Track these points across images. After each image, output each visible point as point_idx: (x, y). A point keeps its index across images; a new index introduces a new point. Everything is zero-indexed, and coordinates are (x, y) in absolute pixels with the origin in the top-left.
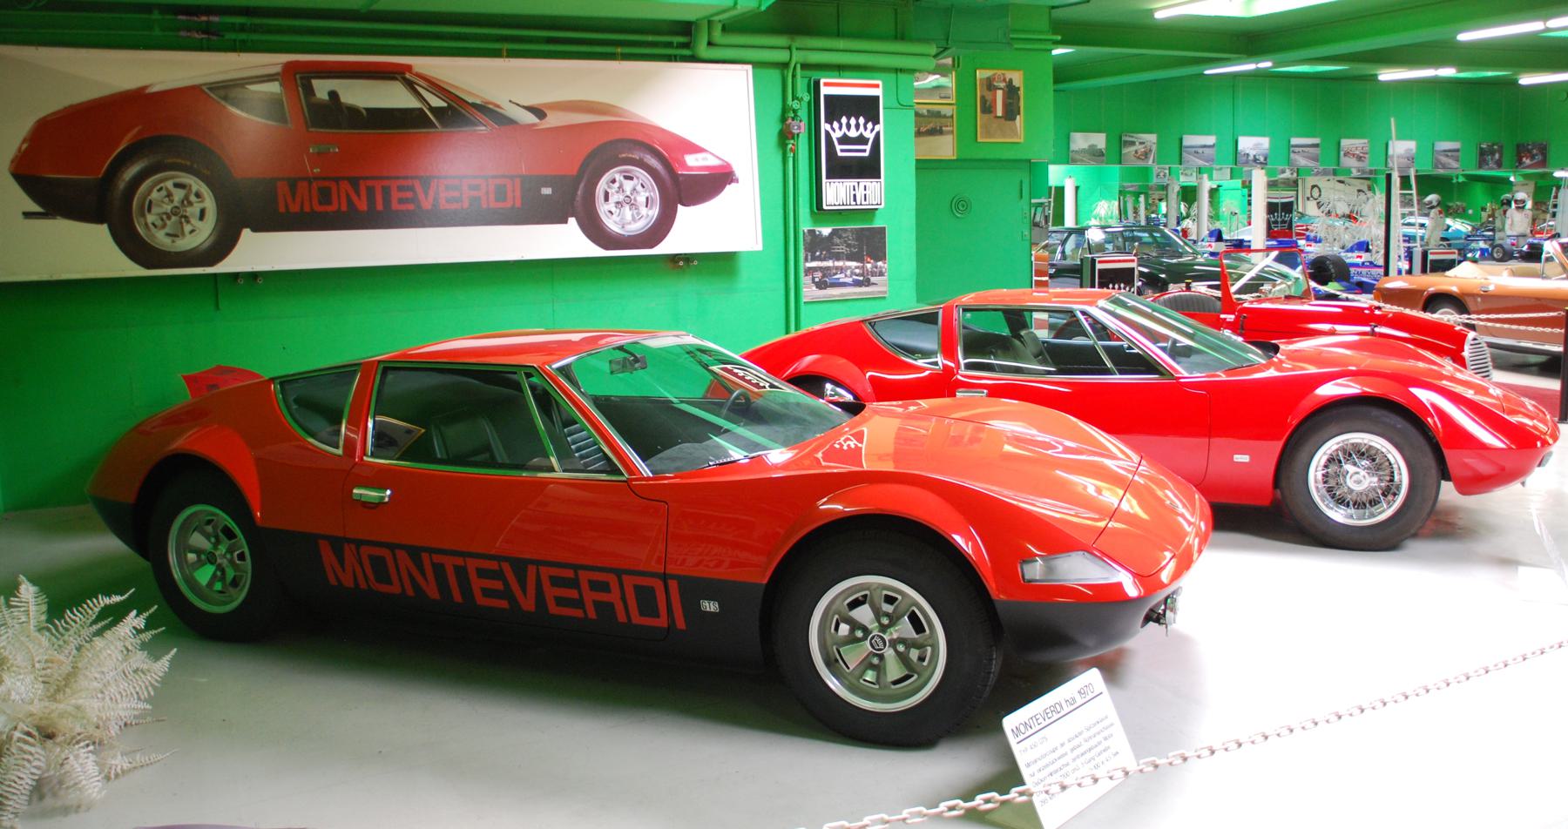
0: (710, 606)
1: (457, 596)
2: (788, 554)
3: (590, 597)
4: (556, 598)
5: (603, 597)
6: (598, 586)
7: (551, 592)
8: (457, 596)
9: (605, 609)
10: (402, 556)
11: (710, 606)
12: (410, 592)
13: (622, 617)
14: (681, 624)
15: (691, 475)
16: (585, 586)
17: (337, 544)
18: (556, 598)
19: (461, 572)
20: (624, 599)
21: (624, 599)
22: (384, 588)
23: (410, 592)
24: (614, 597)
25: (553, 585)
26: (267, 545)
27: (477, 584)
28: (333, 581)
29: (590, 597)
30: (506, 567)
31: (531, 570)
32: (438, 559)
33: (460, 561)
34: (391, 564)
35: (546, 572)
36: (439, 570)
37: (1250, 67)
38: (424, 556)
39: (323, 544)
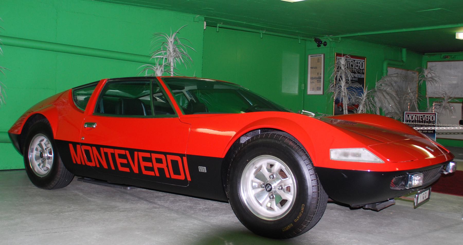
0: (203, 169)
1: (113, 168)
2: (432, 52)
3: (157, 166)
4: (145, 167)
5: (160, 165)
6: (159, 161)
7: (143, 164)
8: (113, 168)
9: (161, 171)
10: (94, 148)
11: (203, 169)
12: (98, 166)
13: (168, 176)
14: (189, 179)
15: (434, 55)
16: (154, 160)
17: (75, 144)
18: (145, 167)
19: (113, 155)
20: (167, 166)
21: (167, 166)
22: (89, 164)
23: (98, 166)
24: (163, 166)
25: (122, 166)
26: (60, 147)
27: (119, 161)
28: (75, 162)
29: (157, 166)
30: (127, 152)
31: (136, 153)
32: (106, 150)
33: (112, 151)
34: (91, 152)
35: (142, 154)
36: (106, 154)
37: (448, 128)
38: (101, 149)
39: (71, 146)
